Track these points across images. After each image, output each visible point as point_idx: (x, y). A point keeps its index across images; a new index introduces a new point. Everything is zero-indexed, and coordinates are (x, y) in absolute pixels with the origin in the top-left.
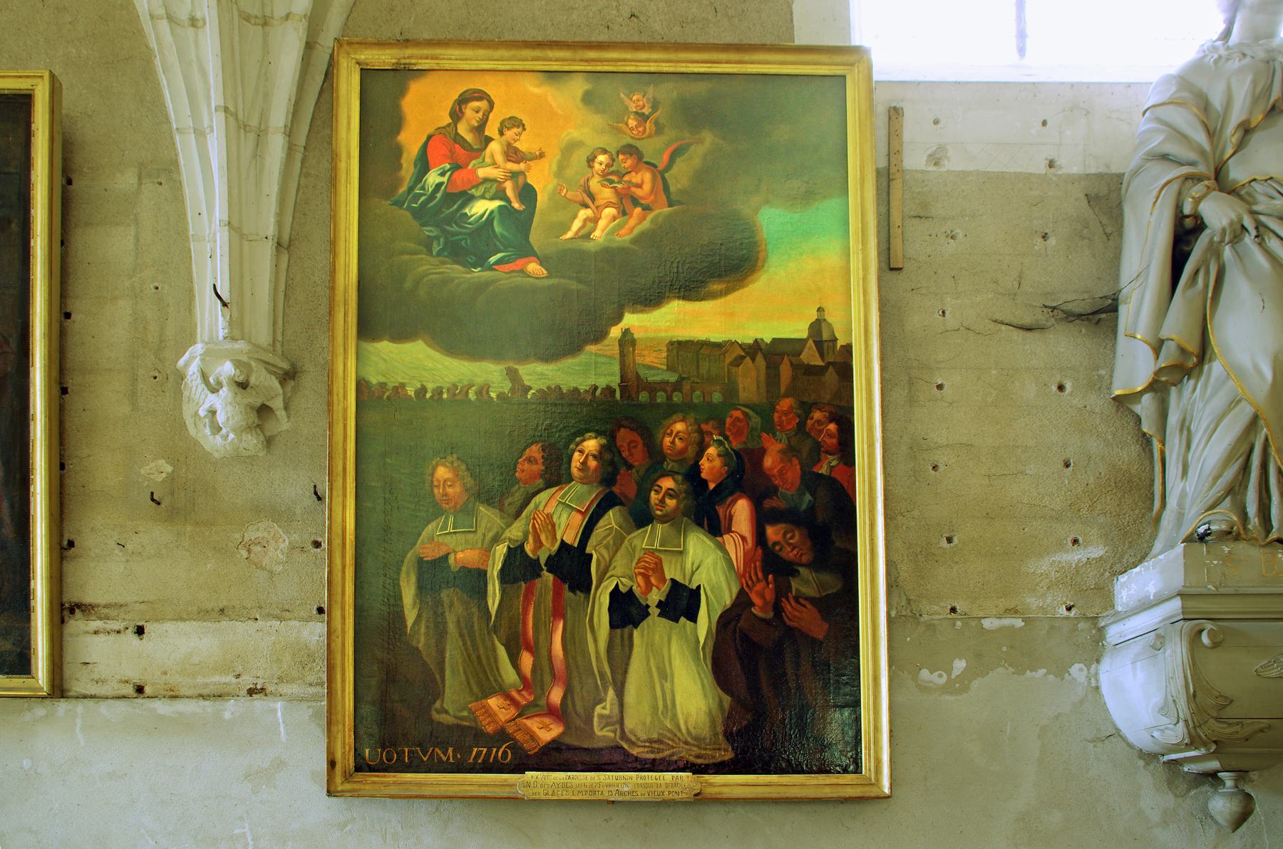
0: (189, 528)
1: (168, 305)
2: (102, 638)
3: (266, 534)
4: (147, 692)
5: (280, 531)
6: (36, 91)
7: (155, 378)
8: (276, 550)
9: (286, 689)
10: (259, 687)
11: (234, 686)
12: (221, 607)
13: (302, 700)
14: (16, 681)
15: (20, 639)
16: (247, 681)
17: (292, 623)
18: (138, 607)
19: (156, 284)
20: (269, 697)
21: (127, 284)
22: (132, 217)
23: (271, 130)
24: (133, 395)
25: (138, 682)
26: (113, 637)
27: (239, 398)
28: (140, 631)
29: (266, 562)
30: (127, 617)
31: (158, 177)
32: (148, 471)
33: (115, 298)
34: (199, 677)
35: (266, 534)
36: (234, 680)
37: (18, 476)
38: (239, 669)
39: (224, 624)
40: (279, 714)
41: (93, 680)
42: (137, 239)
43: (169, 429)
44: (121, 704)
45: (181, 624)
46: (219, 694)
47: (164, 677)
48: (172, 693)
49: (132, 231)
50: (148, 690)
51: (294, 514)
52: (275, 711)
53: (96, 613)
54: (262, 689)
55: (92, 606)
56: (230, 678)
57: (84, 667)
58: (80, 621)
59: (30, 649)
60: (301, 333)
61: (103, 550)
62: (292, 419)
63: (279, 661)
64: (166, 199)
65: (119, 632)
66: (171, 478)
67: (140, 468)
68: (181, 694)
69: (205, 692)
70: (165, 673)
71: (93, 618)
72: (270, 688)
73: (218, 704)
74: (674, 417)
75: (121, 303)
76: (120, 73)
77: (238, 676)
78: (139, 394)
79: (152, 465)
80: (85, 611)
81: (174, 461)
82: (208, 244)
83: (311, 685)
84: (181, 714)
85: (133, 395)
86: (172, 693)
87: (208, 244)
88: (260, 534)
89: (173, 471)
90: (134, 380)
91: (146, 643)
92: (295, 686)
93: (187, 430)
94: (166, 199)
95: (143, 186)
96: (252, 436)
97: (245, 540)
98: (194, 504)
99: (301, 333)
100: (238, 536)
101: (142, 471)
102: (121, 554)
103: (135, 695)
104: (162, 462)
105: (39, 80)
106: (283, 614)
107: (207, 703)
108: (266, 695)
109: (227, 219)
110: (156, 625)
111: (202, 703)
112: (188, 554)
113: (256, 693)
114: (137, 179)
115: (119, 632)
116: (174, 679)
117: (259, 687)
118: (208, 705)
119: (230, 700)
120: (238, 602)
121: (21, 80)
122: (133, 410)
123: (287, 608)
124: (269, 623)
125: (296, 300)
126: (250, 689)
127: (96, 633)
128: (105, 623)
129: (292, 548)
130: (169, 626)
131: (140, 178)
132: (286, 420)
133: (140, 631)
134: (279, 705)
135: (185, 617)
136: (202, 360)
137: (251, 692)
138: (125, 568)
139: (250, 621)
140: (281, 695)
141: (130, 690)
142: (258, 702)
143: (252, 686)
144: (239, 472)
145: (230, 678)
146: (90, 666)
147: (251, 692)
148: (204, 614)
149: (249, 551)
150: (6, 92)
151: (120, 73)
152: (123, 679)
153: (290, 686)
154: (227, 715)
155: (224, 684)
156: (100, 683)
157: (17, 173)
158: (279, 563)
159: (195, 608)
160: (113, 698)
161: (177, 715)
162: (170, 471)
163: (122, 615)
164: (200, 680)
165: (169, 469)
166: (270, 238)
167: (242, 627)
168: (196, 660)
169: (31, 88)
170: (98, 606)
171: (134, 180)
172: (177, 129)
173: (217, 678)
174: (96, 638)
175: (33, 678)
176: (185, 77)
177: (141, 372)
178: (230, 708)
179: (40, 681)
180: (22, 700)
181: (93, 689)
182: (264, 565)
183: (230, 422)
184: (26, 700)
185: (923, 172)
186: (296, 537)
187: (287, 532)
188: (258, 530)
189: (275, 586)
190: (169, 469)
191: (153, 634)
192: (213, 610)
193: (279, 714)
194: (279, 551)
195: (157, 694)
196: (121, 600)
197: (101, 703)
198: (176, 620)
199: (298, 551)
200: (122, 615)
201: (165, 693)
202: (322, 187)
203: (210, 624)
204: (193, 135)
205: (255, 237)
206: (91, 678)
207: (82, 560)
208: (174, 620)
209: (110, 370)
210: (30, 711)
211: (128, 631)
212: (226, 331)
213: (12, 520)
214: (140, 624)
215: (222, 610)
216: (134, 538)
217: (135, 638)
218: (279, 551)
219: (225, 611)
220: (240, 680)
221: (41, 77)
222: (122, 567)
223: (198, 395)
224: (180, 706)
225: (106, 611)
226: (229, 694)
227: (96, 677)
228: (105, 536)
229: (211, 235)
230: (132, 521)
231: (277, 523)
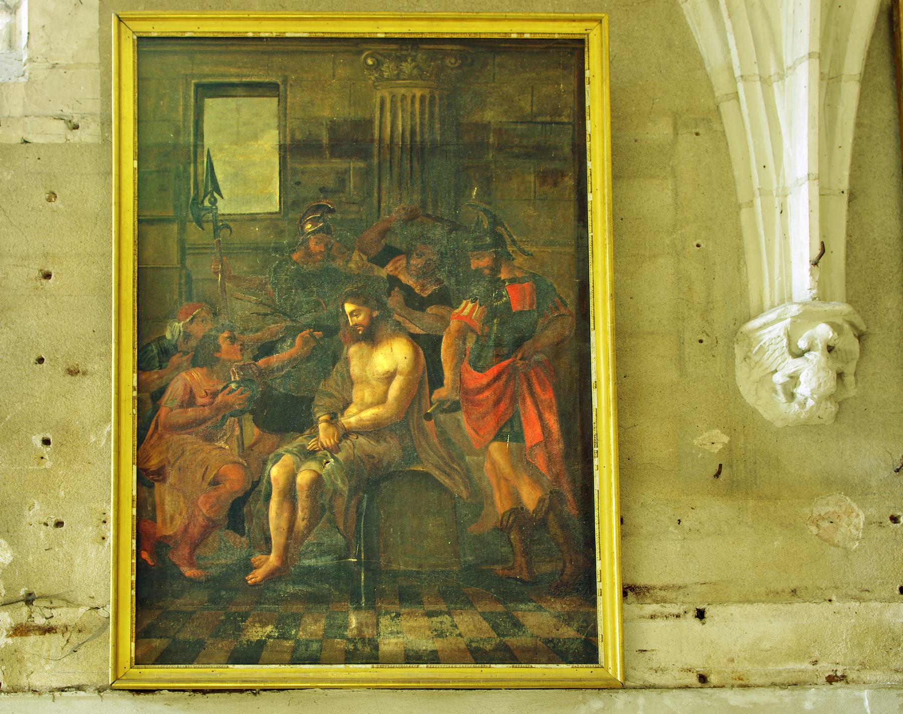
0: (751, 503)
1: (714, 264)
2: (659, 623)
3: (837, 509)
4: (712, 681)
5: (854, 505)
6: (591, 36)
7: (701, 341)
8: (849, 525)
9: (867, 676)
10: (839, 674)
11: (810, 674)
12: (792, 586)
13: (891, 687)
14: (582, 671)
15: (585, 624)
16: (826, 667)
17: (873, 604)
18: (699, 588)
19: (699, 241)
20: (851, 685)
21: (667, 241)
22: (668, 169)
23: (844, 78)
24: (680, 361)
25: (702, 671)
26: (672, 622)
27: (830, 364)
28: (701, 615)
29: (838, 538)
30: (686, 600)
31: (696, 127)
32: (701, 442)
33: (655, 256)
34: (771, 664)
35: (837, 509)
36: (811, 667)
37: (579, 448)
38: (816, 655)
39: (797, 606)
40: (867, 703)
41: (651, 669)
42: (676, 193)
43: (722, 397)
44: (686, 695)
45: (748, 607)
46: (794, 682)
47: (731, 665)
48: (741, 682)
49: (669, 183)
50: (713, 679)
51: (870, 487)
52: (860, 700)
53: (652, 596)
54: (844, 676)
55: (648, 589)
56: (806, 665)
57: (641, 655)
58: (633, 605)
59: (597, 636)
60: (864, 293)
61: (656, 527)
62: (859, 385)
63: (860, 645)
64: (707, 151)
65: (678, 616)
66: (729, 448)
67: (693, 439)
68: (752, 682)
69: (778, 680)
70: (732, 660)
71: (649, 601)
72: (852, 675)
73: (796, 693)
74: (269, 467)
75: (661, 261)
76: (641, 16)
77: (815, 663)
78: (687, 359)
79: (706, 435)
80: (639, 594)
81: (730, 431)
82: (777, 199)
83: (897, 671)
84: (755, 704)
85: (680, 361)
86: (741, 682)
87: (777, 199)
88: (830, 509)
89: (730, 442)
90: (681, 343)
91: (708, 629)
92: (879, 673)
93: (742, 397)
94: (707, 151)
95: (680, 137)
96: (831, 402)
97: (814, 515)
98: (756, 478)
99: (864, 293)
100: (807, 510)
101: (695, 442)
102: (676, 531)
103: (699, 685)
104: (716, 432)
105: (595, 24)
106: (862, 595)
107: (785, 692)
108: (847, 683)
109: (817, 172)
110: (719, 608)
111: (779, 692)
112: (752, 531)
113: (837, 681)
114: (672, 129)
115: (678, 616)
116: (744, 667)
117: (839, 674)
118: (785, 695)
119: (811, 688)
120: (811, 582)
121: (574, 24)
122: (681, 376)
123: (866, 587)
124: (847, 605)
125: (856, 257)
126: (829, 676)
127: (652, 617)
128: (662, 606)
129: (869, 523)
130: (734, 610)
131: (675, 128)
132: (854, 386)
133: (701, 615)
134: (865, 694)
135: (752, 599)
136: (793, 323)
137: (831, 680)
138: (682, 547)
139: (825, 603)
140: (864, 683)
141: (693, 680)
142: (841, 691)
143: (831, 673)
144: (804, 441)
145: (806, 665)
146: (647, 653)
147: (831, 680)
148: (773, 596)
149: (818, 526)
150: (556, 36)
151: (641, 16)
152: (685, 667)
153: (873, 672)
154: (808, 706)
155: (799, 671)
156: (660, 673)
157: (569, 123)
158: (853, 540)
159: (763, 590)
160: (675, 688)
161: (752, 706)
162: (726, 442)
163: (681, 598)
164: (772, 667)
165: (726, 439)
166: (846, 192)
167: (818, 610)
168: (766, 645)
169: (585, 32)
170: (654, 588)
171: (669, 130)
172: (742, 76)
173: (791, 665)
174: (653, 624)
175: (602, 667)
176: (751, 22)
177: (687, 335)
178: (811, 698)
179: (610, 671)
180: (578, 692)
181: (653, 679)
182: (836, 541)
183: (822, 389)
184: (581, 691)
185: (203, 145)
186: (872, 511)
187: (862, 506)
188: (828, 504)
189: (851, 565)
190: (726, 439)
191: (716, 618)
192: (783, 591)
193: (867, 703)
194: (852, 527)
195: (724, 682)
196: (679, 581)
197: (664, 694)
198: (743, 602)
199: (874, 526)
200: (681, 598)
201: (734, 682)
202: (877, 138)
203: (780, 606)
204: (759, 83)
205: (828, 192)
206: (650, 666)
207: (633, 538)
208: (740, 602)
209: (653, 333)
210: (585, 703)
211: (687, 615)
212: (815, 291)
213: (575, 495)
214: (701, 607)
215: (794, 591)
216: (690, 514)
217: (696, 622)
218: (852, 527)
219: (798, 593)
220: (817, 667)
221: (600, 21)
222: (679, 545)
223: (771, 359)
224: (753, 696)
225: (663, 593)
226: (805, 683)
227: (655, 665)
228: (658, 511)
229: (780, 190)
230: (687, 495)
231: (850, 496)
